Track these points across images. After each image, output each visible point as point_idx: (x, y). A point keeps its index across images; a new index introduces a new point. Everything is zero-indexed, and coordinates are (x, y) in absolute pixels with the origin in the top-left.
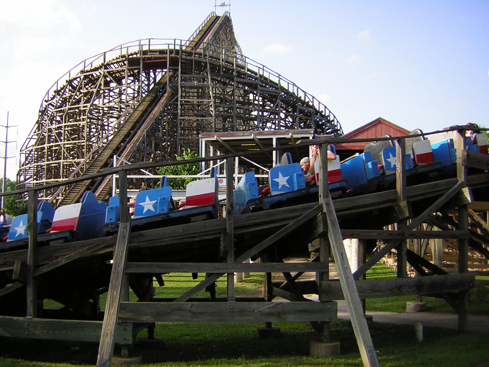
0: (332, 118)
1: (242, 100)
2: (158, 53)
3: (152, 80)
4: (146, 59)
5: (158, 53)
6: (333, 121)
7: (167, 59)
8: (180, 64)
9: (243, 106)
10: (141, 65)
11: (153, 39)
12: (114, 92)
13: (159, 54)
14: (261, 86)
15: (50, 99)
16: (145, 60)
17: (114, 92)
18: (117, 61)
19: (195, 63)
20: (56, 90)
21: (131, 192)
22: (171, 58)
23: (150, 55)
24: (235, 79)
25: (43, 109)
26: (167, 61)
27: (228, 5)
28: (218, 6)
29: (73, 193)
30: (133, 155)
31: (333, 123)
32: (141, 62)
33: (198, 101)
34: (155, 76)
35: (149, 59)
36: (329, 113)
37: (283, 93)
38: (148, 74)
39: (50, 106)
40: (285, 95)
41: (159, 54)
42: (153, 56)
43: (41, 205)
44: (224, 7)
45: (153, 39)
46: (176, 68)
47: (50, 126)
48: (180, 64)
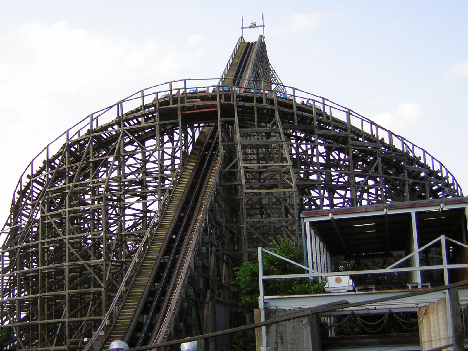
0: (450, 181)
1: (324, 161)
2: (200, 100)
3: (189, 139)
4: (185, 109)
5: (200, 100)
6: (453, 184)
7: (217, 107)
8: (236, 113)
9: (326, 169)
10: (180, 117)
11: (190, 79)
12: (135, 159)
13: (201, 101)
14: (353, 139)
15: (35, 173)
16: (185, 111)
17: (135, 159)
18: (134, 116)
19: (257, 110)
20: (46, 160)
21: (305, 298)
22: (222, 105)
23: (188, 102)
24: (317, 131)
25: (23, 188)
26: (217, 110)
27: (261, 26)
28: (246, 28)
29: (127, 309)
30: (198, 248)
31: (452, 187)
32: (179, 113)
33: (259, 166)
34: (193, 133)
35: (189, 108)
36: (447, 174)
37: (383, 148)
38: (185, 131)
39: (35, 184)
40: (387, 150)
41: (201, 101)
42: (194, 103)
43: (102, 326)
44: (256, 28)
45: (190, 79)
46: (231, 119)
47: (63, 212)
48: (236, 113)
